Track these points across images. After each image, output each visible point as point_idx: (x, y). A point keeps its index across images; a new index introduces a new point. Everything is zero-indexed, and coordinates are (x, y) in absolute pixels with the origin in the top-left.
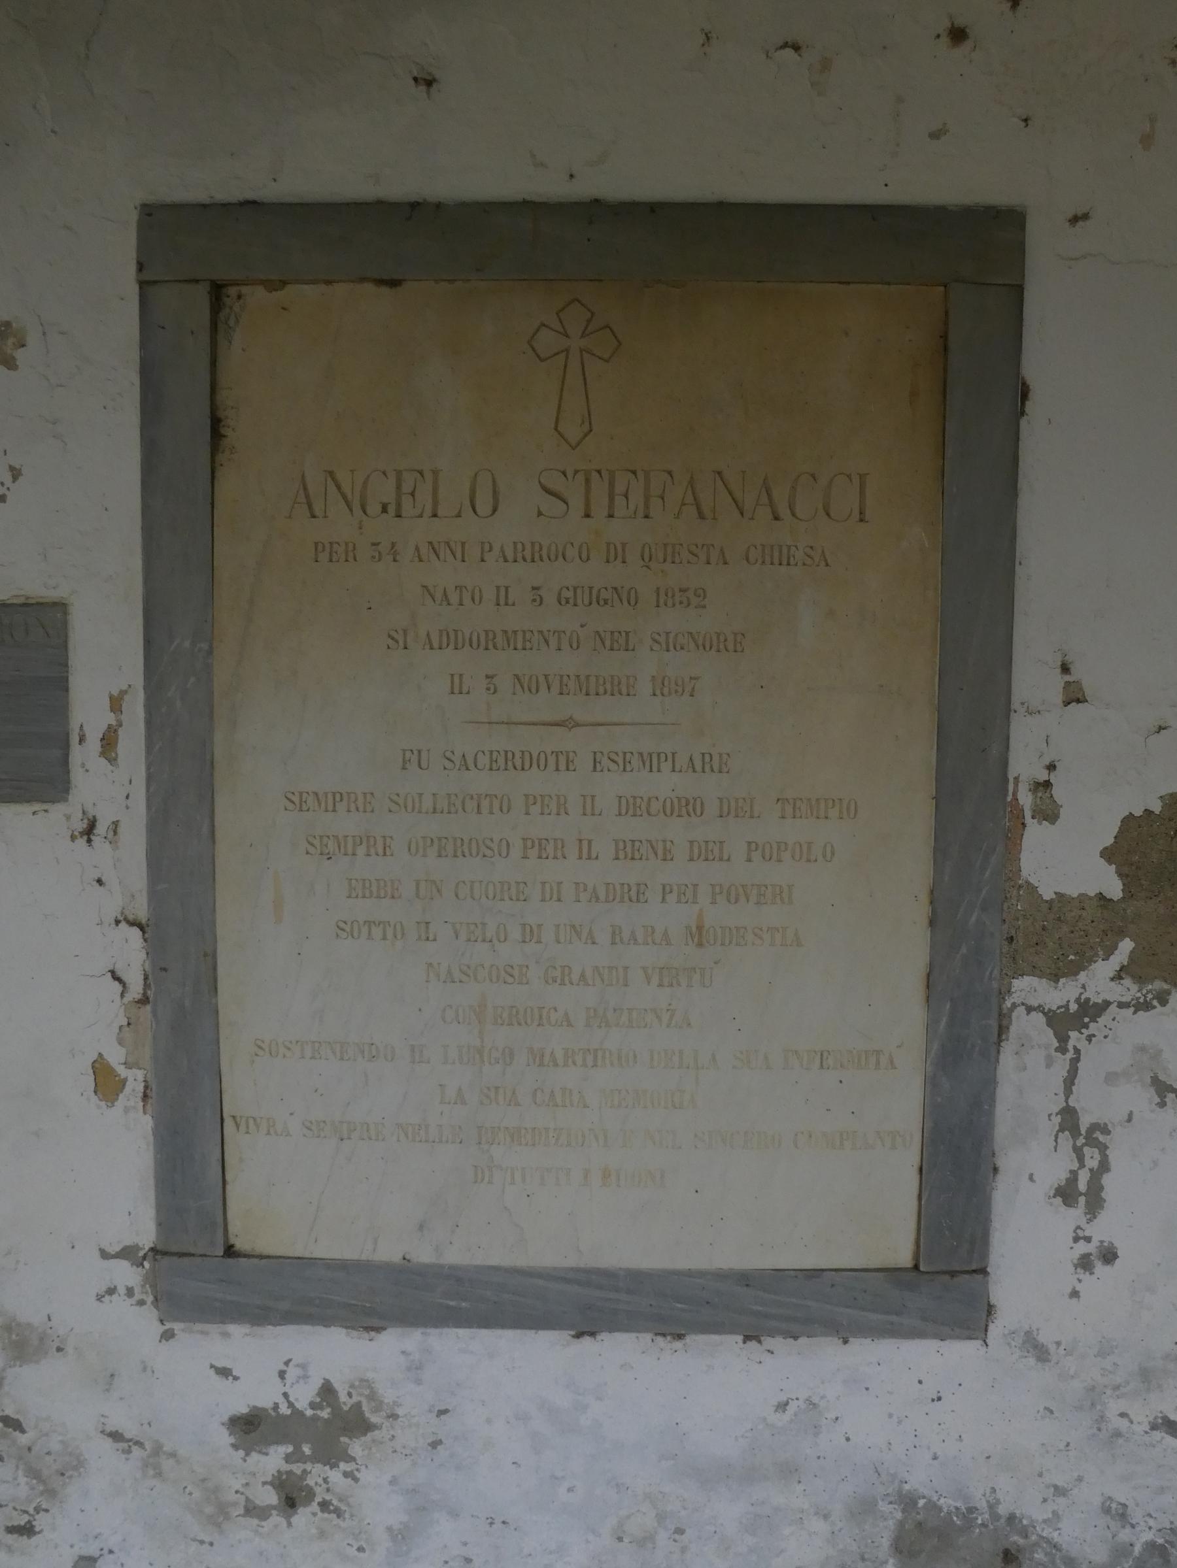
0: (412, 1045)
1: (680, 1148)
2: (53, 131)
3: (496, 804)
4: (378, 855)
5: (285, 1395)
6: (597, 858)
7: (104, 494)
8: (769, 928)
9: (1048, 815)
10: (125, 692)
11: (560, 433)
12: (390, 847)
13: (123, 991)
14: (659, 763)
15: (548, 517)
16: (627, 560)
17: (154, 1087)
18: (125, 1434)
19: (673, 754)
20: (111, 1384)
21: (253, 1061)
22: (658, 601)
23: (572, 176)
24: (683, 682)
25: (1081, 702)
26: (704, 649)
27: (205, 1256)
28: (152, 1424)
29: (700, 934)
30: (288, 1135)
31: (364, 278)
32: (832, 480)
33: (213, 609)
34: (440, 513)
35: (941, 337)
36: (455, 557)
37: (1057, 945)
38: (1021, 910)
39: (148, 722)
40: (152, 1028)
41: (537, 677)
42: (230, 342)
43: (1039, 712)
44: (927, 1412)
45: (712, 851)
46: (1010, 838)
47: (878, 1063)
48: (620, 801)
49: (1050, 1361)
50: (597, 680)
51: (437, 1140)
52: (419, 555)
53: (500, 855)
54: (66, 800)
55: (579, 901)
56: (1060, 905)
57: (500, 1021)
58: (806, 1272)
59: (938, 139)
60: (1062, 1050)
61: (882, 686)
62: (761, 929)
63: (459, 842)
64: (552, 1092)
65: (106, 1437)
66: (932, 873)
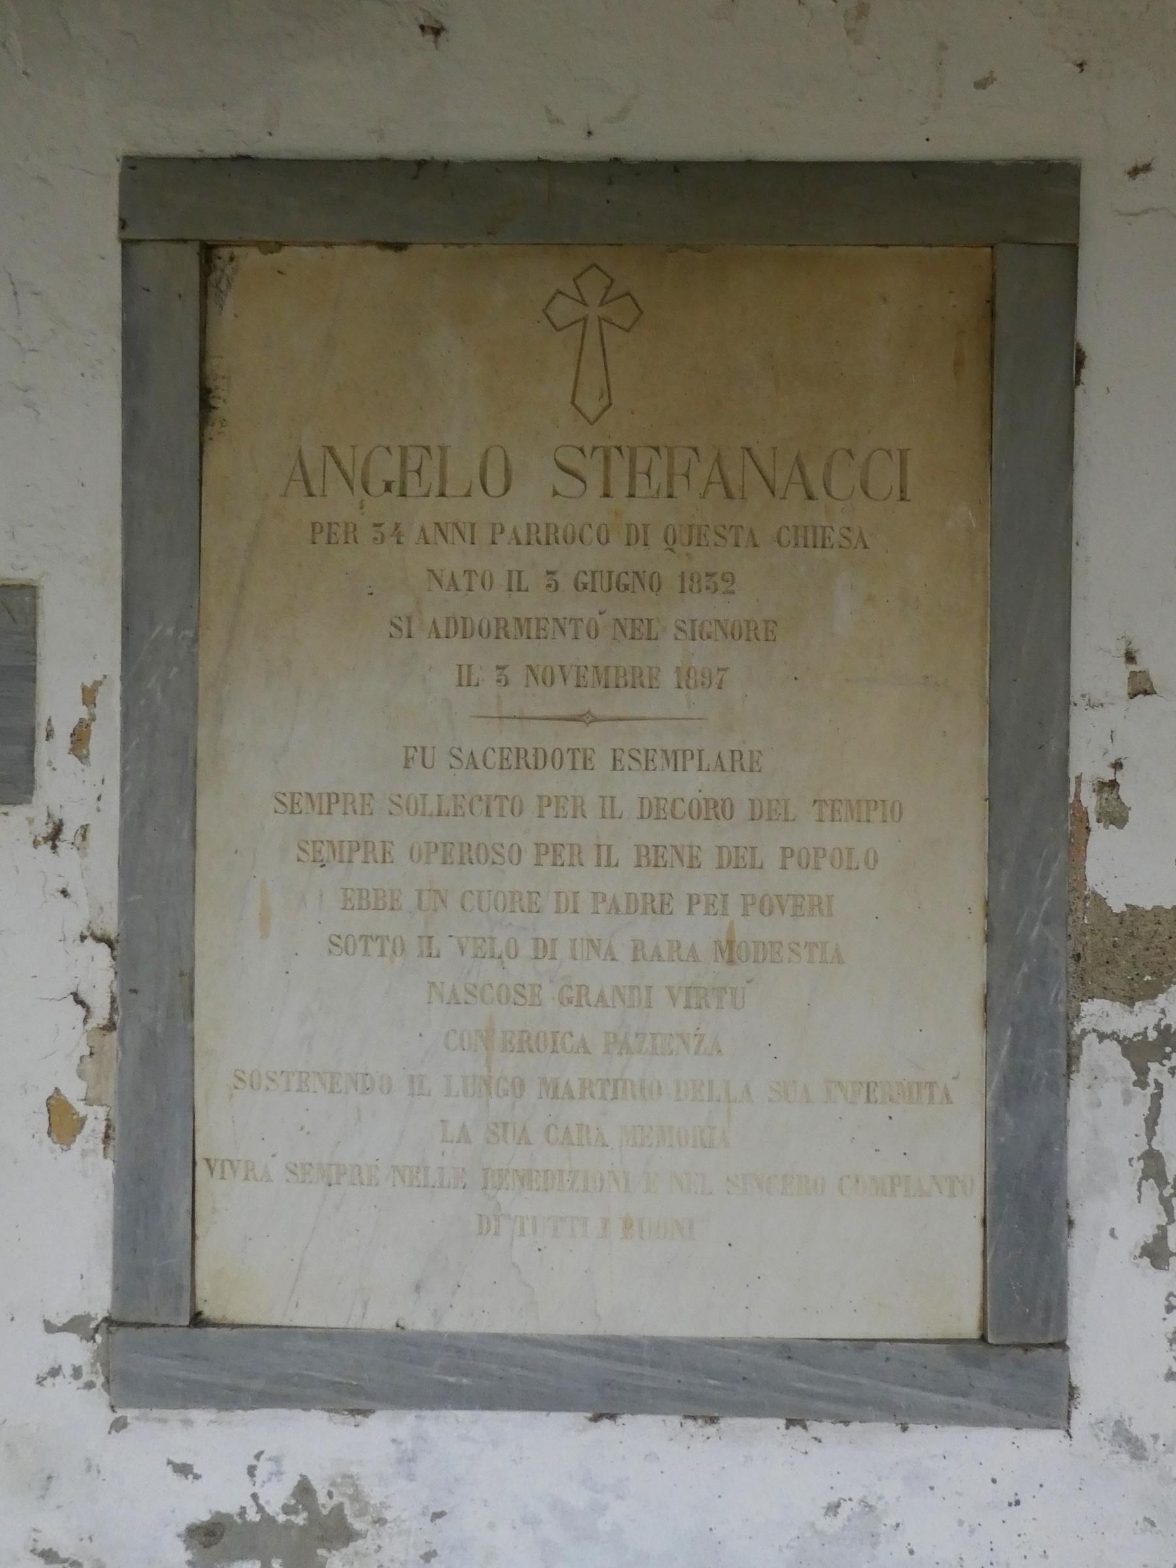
0: (411, 1076)
1: (711, 1193)
2: (25, 73)
3: (507, 805)
4: (377, 862)
5: (255, 1496)
6: (617, 865)
7: (81, 469)
8: (806, 943)
9: (1115, 818)
10: (100, 683)
11: (577, 408)
12: (389, 853)
13: (86, 1016)
14: (684, 762)
15: (564, 496)
16: (649, 543)
17: (117, 1127)
18: (59, 1553)
19: (700, 751)
20: (47, 1489)
21: (232, 1095)
22: (682, 585)
23: (590, 133)
24: (710, 674)
25: (1149, 694)
26: (733, 638)
27: (168, 1326)
28: (93, 1538)
29: (731, 949)
30: (269, 1180)
31: (367, 241)
32: (870, 456)
33: (199, 593)
34: (447, 492)
35: (988, 302)
36: (463, 539)
37: (1131, 964)
38: (1087, 925)
39: (125, 716)
40: (117, 1058)
41: (552, 668)
42: (221, 307)
43: (1102, 705)
44: (1004, 1519)
45: (743, 857)
46: (1073, 844)
47: (932, 1096)
48: (642, 803)
49: (1147, 1459)
50: (617, 671)
51: (437, 1185)
52: (425, 537)
53: (511, 862)
54: (29, 802)
55: (597, 913)
56: (1132, 918)
57: (509, 1048)
58: (856, 1342)
59: (984, 89)
60: (1142, 1083)
61: (927, 677)
62: (798, 945)
63: (466, 847)
64: (567, 1128)
65: (36, 1557)
66: (987, 883)
